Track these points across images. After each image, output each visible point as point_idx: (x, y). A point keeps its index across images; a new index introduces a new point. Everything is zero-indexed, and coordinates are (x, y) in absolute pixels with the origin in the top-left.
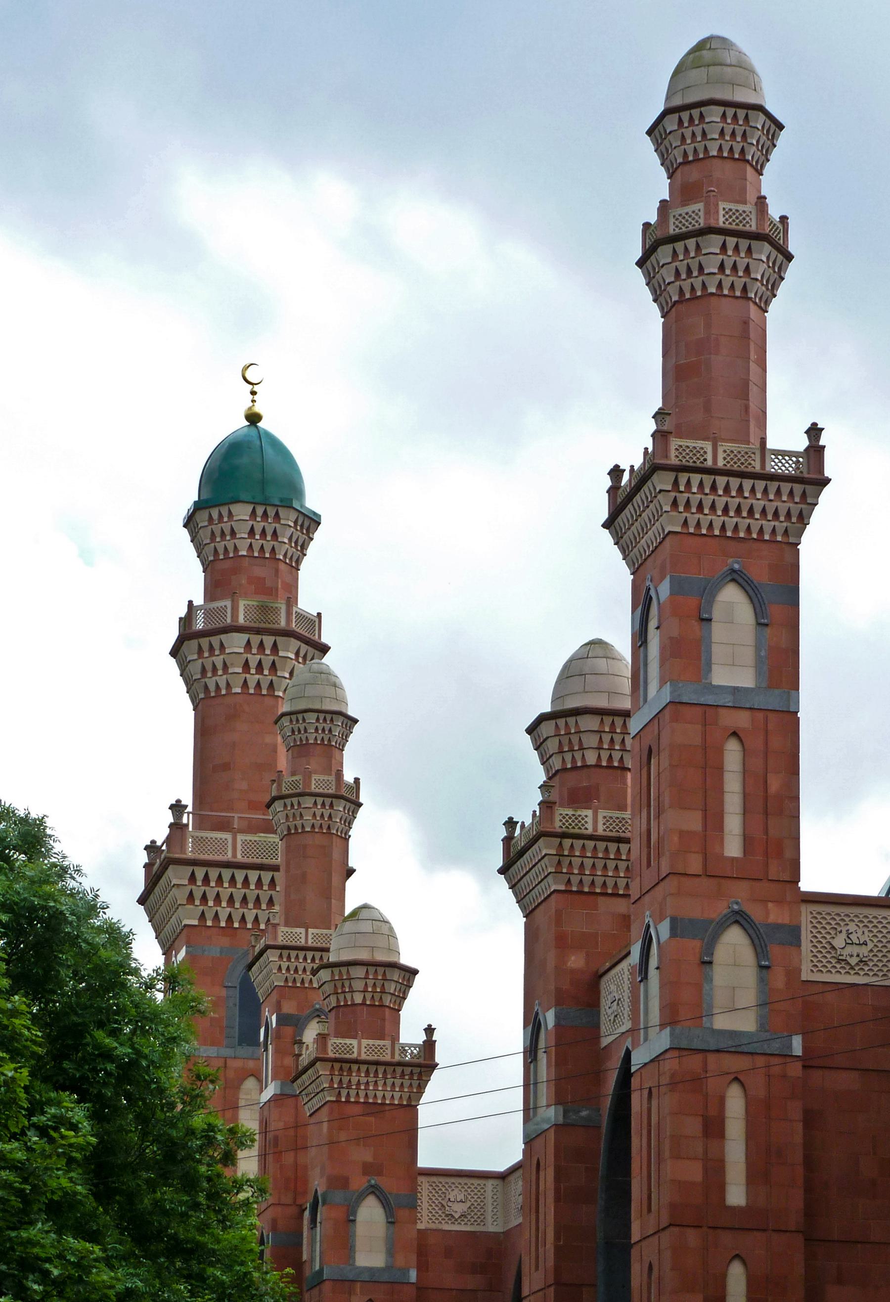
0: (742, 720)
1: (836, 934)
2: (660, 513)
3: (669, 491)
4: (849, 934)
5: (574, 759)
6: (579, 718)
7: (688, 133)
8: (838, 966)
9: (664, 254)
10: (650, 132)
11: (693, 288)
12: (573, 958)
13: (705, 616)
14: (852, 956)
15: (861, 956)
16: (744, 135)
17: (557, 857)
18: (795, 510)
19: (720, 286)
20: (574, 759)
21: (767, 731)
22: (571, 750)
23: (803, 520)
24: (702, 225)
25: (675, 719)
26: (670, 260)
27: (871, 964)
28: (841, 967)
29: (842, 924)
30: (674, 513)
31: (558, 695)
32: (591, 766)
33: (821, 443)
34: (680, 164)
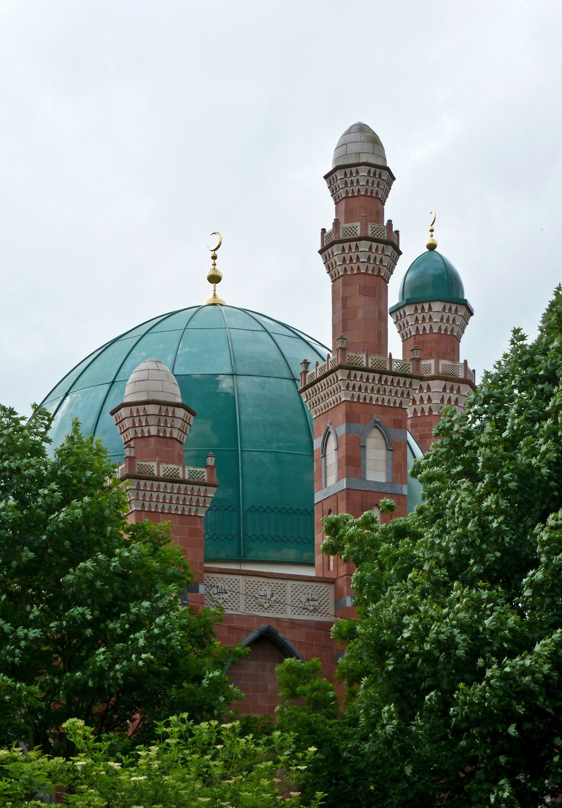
2: (339, 389)
5: (183, 510)
9: (336, 249)
10: (326, 177)
13: (363, 445)
14: (310, 606)
20: (183, 510)
34: (344, 198)
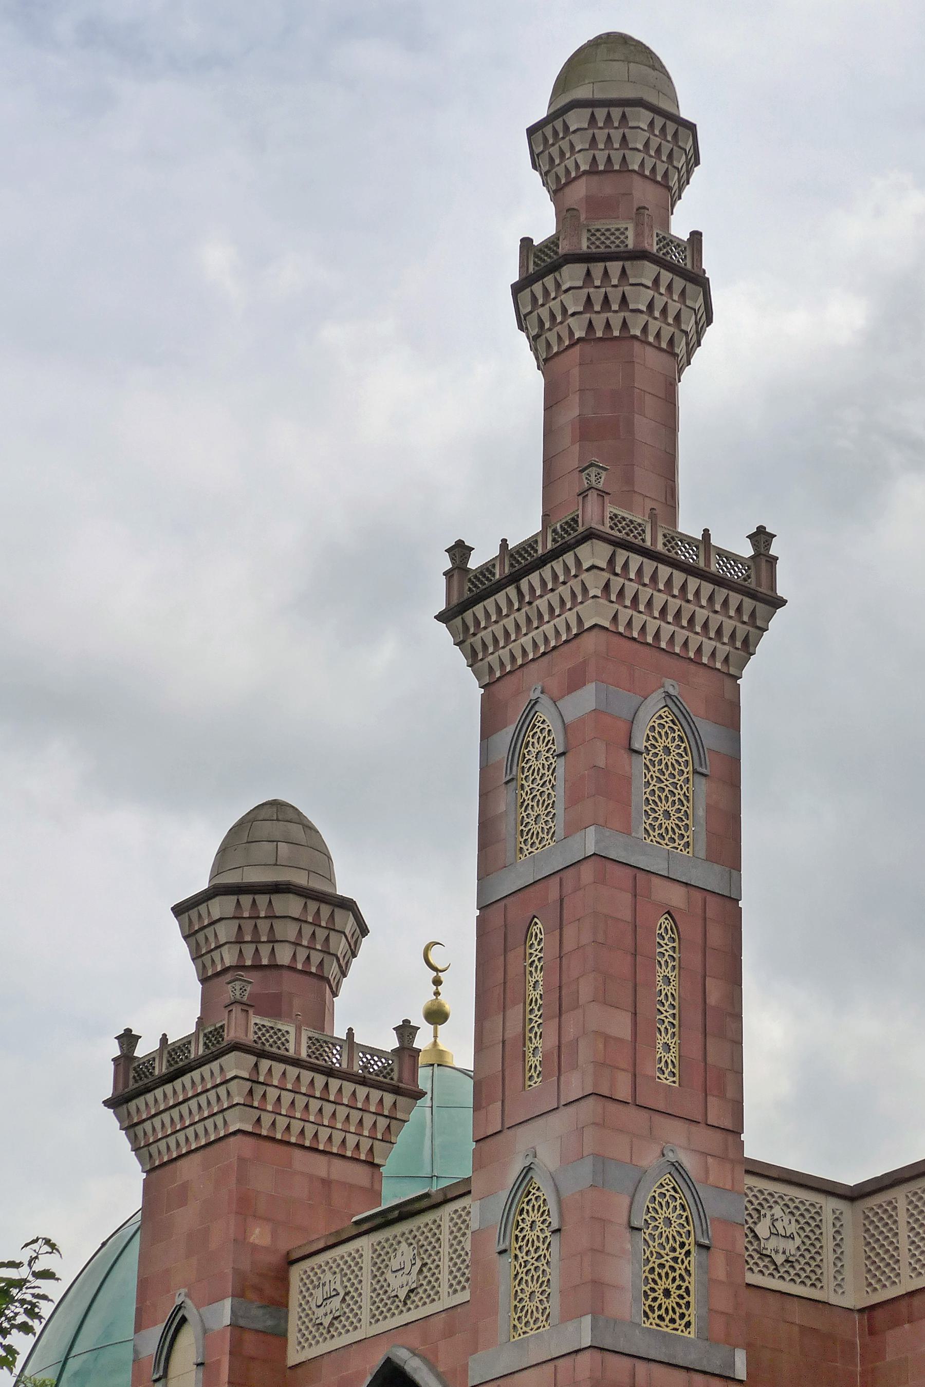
0: (676, 897)
1: (759, 1218)
3: (603, 570)
4: (774, 1220)
6: (274, 897)
7: (601, 136)
8: (761, 1264)
11: (608, 325)
12: (257, 1231)
14: (777, 1252)
15: (788, 1253)
16: (670, 156)
17: (249, 1084)
18: (742, 630)
19: (645, 329)
21: (705, 919)
22: (256, 941)
23: (748, 648)
24: (631, 246)
25: (601, 879)
26: (580, 284)
27: (798, 1267)
28: (765, 1266)
29: (766, 1205)
30: (603, 601)
31: (219, 866)
32: (282, 966)
33: (772, 552)
